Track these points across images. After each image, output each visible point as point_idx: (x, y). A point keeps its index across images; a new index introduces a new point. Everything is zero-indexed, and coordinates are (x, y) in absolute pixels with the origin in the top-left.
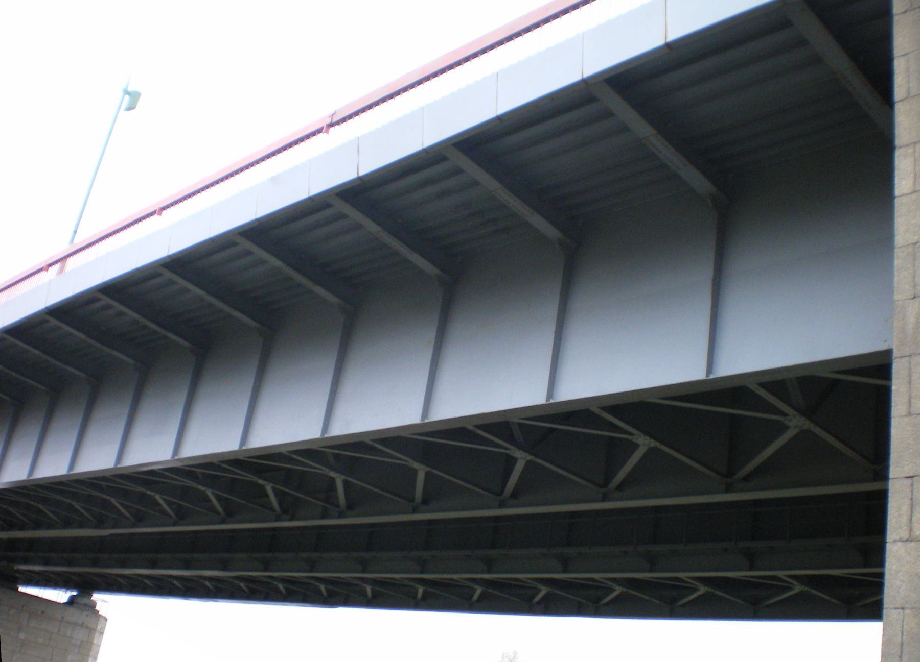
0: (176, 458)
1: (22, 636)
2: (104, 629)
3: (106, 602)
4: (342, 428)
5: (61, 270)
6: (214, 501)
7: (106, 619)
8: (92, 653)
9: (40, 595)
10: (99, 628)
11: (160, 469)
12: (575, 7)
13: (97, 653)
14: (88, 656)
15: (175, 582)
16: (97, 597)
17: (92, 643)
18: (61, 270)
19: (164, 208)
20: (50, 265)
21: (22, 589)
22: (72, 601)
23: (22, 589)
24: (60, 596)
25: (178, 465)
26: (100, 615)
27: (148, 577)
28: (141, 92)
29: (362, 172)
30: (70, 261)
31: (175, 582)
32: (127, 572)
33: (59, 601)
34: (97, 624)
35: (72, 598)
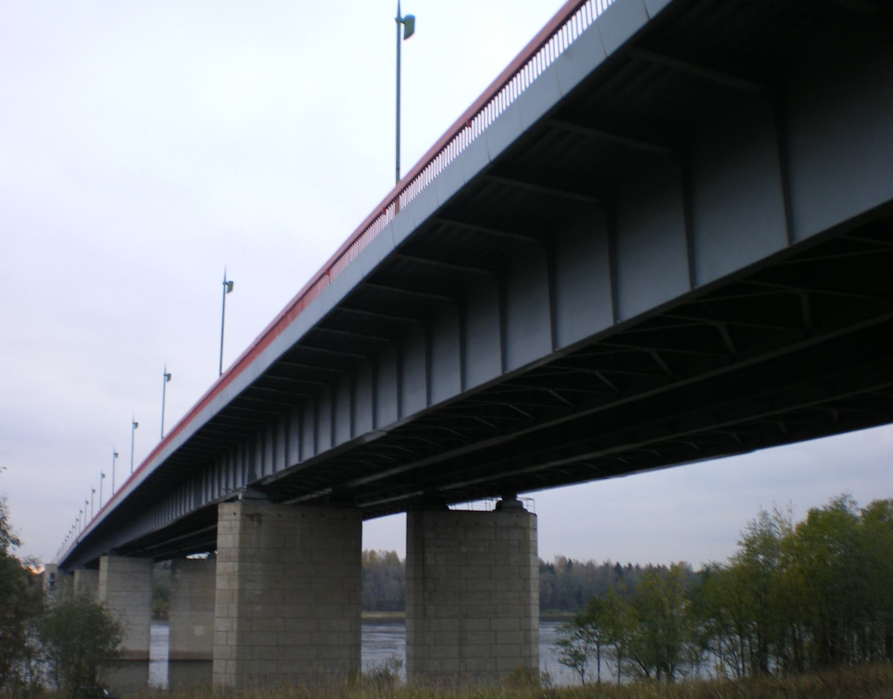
0: (557, 350)
1: (464, 550)
2: (536, 525)
3: (530, 499)
4: (706, 278)
5: (397, 209)
6: (605, 380)
7: (535, 515)
8: (532, 550)
9: (470, 509)
10: (531, 525)
11: (545, 365)
12: (578, 8)
13: (536, 548)
14: (529, 553)
15: (562, 471)
16: (520, 497)
17: (529, 540)
18: (397, 209)
19: (472, 118)
20: (387, 207)
21: (452, 507)
22: (209, 557)
23: (452, 507)
24: (204, 556)
25: (560, 356)
26: (529, 513)
27: (564, 467)
28: (118, 453)
29: (653, 12)
30: (334, 271)
31: (562, 471)
32: (542, 467)
33: (488, 510)
34: (529, 522)
35: (499, 505)
